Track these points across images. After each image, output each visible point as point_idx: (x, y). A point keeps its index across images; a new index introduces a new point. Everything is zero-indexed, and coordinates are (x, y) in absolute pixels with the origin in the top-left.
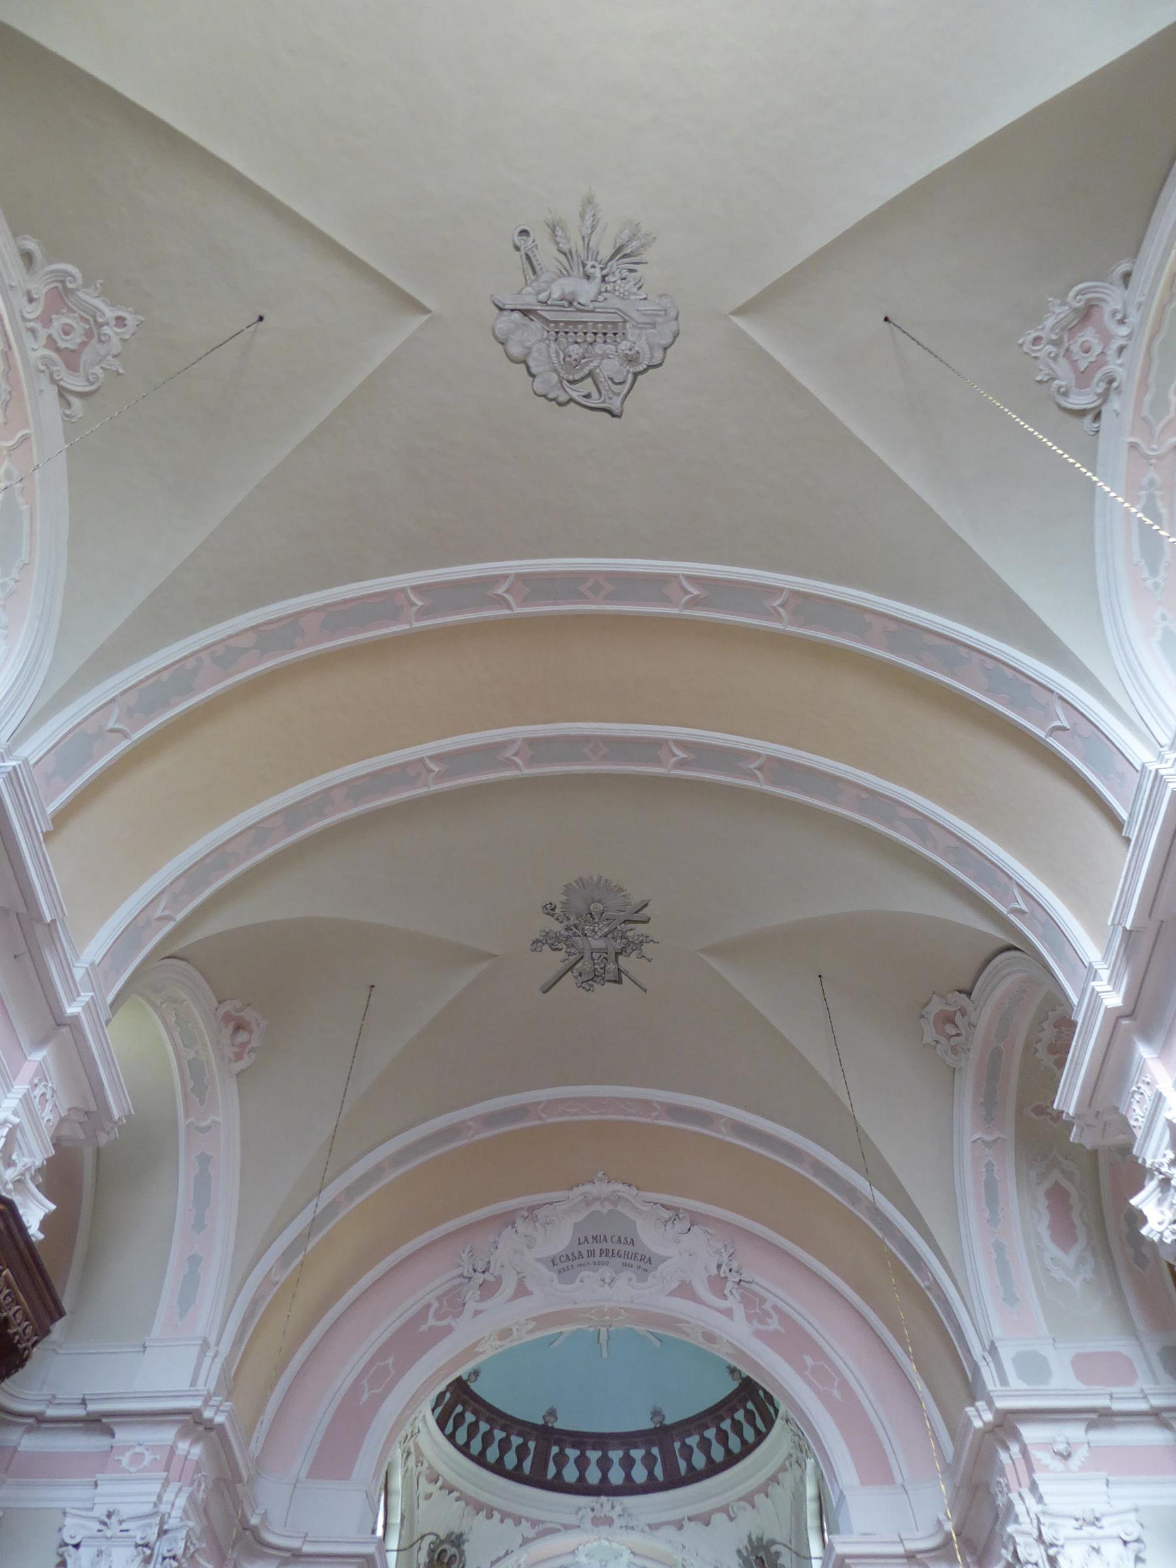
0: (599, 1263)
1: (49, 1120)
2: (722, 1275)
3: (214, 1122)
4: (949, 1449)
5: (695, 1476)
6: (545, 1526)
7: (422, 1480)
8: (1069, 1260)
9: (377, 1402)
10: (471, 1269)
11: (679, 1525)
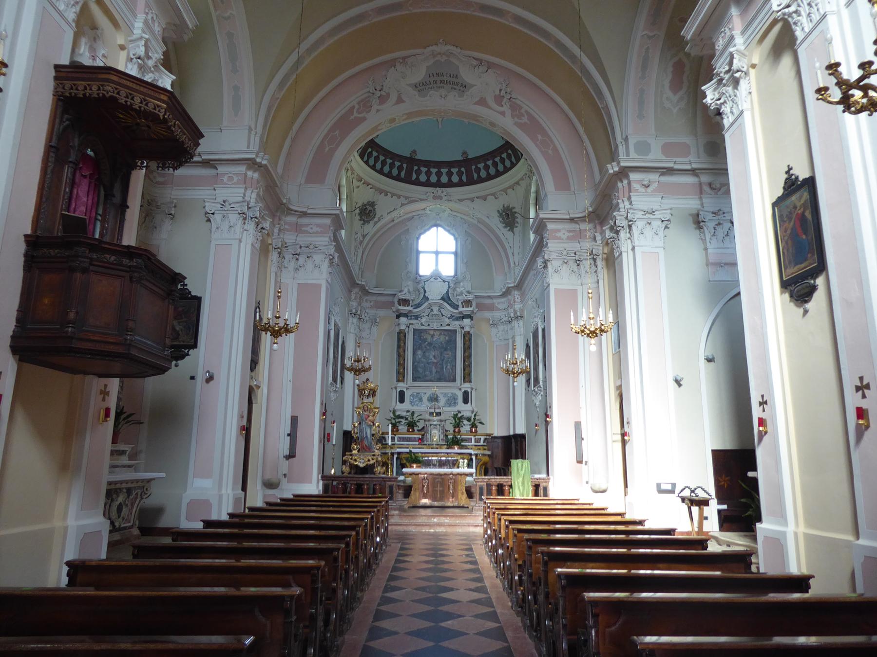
0: (439, 87)
1: (158, 31)
2: (502, 95)
3: (231, 14)
4: (597, 177)
5: (481, 180)
6: (411, 199)
7: (355, 181)
8: (675, 98)
9: (333, 151)
10: (374, 89)
11: (472, 200)
